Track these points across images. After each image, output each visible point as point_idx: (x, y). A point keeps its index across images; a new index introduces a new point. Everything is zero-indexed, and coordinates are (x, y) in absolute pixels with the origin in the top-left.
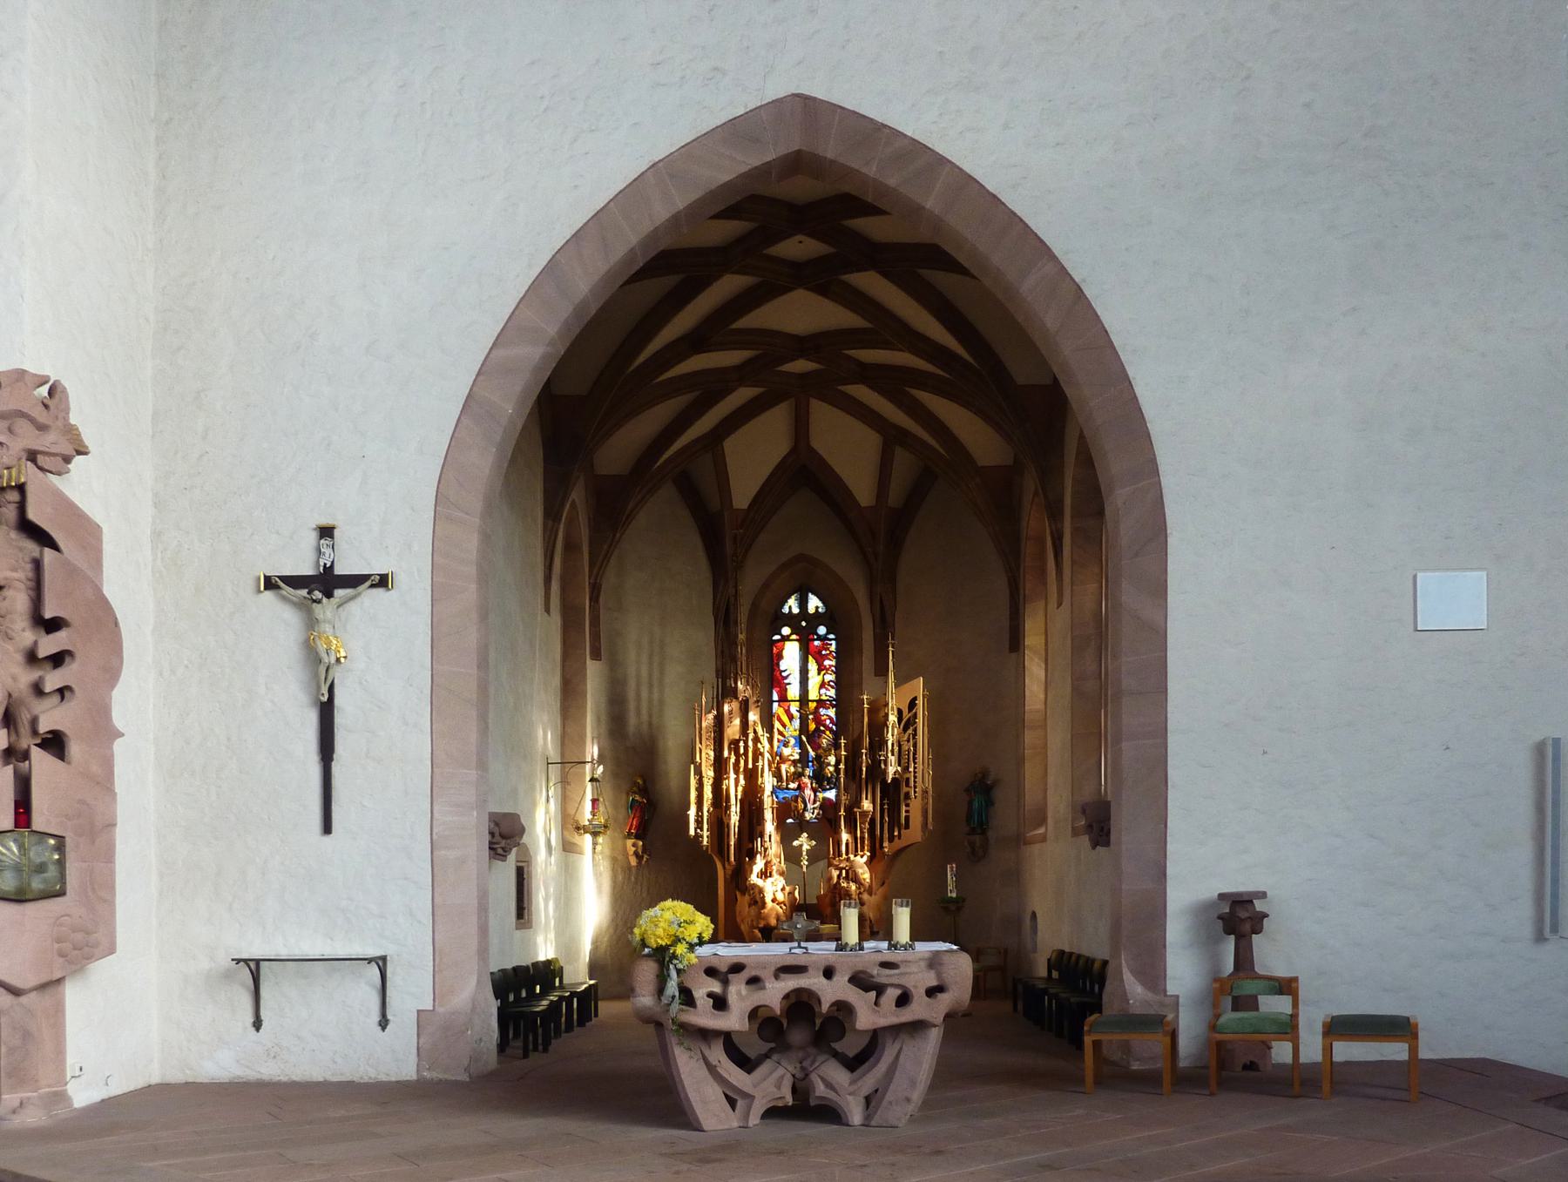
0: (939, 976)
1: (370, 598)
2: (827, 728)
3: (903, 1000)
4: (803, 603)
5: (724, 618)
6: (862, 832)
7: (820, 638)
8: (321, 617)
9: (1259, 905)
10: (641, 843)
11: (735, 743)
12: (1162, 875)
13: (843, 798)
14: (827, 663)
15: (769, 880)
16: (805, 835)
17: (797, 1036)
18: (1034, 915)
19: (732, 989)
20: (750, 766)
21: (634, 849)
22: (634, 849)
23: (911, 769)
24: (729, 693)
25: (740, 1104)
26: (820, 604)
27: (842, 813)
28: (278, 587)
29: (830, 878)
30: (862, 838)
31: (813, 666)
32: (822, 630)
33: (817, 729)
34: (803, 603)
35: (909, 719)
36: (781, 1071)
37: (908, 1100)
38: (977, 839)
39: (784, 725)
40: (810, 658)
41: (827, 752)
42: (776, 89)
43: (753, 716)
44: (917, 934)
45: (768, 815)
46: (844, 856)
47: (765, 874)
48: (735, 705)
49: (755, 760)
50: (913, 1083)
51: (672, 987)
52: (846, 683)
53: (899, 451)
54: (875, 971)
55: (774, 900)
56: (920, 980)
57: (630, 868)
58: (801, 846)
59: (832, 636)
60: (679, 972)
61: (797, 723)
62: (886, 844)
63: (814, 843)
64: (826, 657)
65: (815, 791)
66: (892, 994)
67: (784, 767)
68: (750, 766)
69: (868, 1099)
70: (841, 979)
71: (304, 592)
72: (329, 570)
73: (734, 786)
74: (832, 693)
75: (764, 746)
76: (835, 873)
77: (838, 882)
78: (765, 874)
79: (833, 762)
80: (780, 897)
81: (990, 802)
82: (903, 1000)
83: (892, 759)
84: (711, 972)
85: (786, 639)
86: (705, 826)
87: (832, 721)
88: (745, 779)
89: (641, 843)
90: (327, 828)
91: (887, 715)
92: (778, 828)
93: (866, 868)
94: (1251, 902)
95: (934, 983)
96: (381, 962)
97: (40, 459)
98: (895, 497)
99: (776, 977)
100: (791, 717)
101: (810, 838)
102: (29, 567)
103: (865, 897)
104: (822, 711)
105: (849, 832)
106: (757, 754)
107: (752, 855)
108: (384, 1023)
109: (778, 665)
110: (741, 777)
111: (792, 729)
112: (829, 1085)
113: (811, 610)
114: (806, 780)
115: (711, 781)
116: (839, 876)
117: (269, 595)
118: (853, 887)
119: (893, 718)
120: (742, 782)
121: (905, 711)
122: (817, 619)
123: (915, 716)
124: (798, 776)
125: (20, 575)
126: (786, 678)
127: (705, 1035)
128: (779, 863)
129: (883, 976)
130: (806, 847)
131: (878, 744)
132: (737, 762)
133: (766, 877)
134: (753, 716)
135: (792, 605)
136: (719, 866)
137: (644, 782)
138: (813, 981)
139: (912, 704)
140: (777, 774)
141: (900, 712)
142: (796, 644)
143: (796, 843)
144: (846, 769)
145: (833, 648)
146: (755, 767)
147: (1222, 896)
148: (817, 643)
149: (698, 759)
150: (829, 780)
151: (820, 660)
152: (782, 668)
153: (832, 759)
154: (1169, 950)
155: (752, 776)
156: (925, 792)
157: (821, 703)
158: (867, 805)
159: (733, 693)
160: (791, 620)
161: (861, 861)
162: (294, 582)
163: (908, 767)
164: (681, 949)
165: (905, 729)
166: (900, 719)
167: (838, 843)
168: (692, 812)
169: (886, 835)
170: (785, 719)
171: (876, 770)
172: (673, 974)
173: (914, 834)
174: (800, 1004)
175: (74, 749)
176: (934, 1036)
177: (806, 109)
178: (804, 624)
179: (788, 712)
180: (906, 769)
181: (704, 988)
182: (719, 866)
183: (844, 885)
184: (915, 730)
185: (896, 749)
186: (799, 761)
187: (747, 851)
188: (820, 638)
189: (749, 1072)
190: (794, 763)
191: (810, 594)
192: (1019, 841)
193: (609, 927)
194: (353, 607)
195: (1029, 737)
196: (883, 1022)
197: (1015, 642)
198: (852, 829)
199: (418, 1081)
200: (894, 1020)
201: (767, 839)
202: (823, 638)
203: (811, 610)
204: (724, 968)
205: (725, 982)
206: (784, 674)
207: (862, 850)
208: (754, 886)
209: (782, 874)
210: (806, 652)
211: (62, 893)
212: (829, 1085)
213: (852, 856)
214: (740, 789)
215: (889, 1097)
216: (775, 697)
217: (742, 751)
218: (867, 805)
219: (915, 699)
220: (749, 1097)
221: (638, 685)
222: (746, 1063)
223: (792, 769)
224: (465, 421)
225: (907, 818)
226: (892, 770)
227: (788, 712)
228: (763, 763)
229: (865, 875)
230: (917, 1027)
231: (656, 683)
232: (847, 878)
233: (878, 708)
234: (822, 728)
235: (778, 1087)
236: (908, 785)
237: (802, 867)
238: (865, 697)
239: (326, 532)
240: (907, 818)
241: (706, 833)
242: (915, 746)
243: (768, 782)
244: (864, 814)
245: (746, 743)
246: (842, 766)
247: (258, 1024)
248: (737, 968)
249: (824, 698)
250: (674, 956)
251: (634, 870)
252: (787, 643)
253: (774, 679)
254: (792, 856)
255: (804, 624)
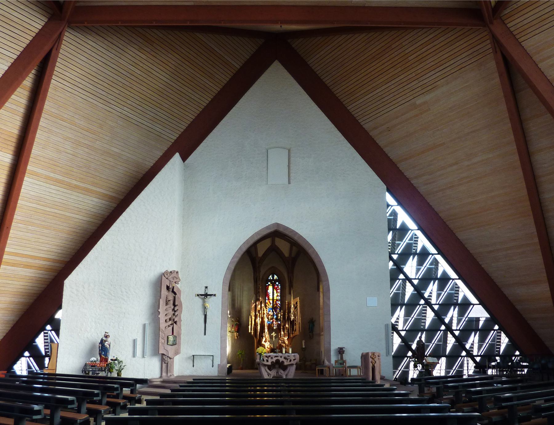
0: (295, 357)
1: (213, 297)
2: (278, 306)
3: (290, 361)
4: (273, 277)
5: (256, 281)
6: (286, 332)
7: (277, 285)
8: (206, 301)
9: (344, 349)
10: (238, 334)
11: (259, 311)
12: (330, 344)
13: (282, 324)
14: (278, 291)
15: (266, 343)
16: (274, 332)
17: (277, 366)
18: (322, 351)
19: (269, 359)
20: (262, 316)
21: (236, 335)
22: (236, 335)
23: (296, 318)
24: (257, 300)
25: (269, 376)
26: (277, 277)
27: (282, 327)
28: (199, 296)
29: (279, 343)
30: (286, 333)
31: (275, 291)
32: (277, 283)
33: (276, 306)
34: (273, 277)
35: (296, 307)
36: (275, 371)
37: (291, 375)
38: (311, 334)
39: (269, 305)
40: (275, 289)
41: (279, 313)
42: (273, 222)
43: (263, 305)
44: (292, 353)
45: (266, 328)
46: (282, 338)
47: (265, 342)
48: (259, 302)
49: (263, 315)
50: (292, 373)
51: (262, 359)
52: (282, 295)
53: (294, 247)
54: (287, 357)
55: (267, 348)
56: (292, 358)
57: (235, 339)
58: (273, 335)
59: (279, 285)
60: (263, 356)
61: (272, 305)
62: (291, 335)
63: (276, 334)
64: (278, 289)
65: (276, 322)
66: (289, 360)
67: (269, 317)
68: (262, 316)
69: (286, 375)
70: (283, 358)
71: (204, 297)
72: (207, 293)
73: (259, 321)
74: (279, 298)
75: (265, 312)
76: (280, 341)
77: (281, 344)
78: (265, 342)
79: (280, 316)
80: (269, 347)
81: (314, 325)
82: (290, 361)
83: (292, 315)
84: (266, 357)
85: (269, 285)
86: (253, 330)
87: (279, 305)
88: (261, 319)
89: (238, 334)
90: (205, 334)
91: (291, 305)
92: (268, 331)
93: (287, 340)
94: (342, 349)
95: (294, 359)
96: (213, 356)
97: (176, 283)
98: (293, 255)
99: (275, 357)
100: (270, 303)
101: (275, 333)
102: (173, 297)
103: (287, 347)
104: (277, 302)
105: (283, 332)
106: (264, 314)
107: (262, 337)
108: (213, 366)
109: (267, 291)
110: (260, 319)
111: (270, 306)
112: (281, 373)
113: (275, 278)
114: (274, 320)
115: (254, 320)
116: (281, 342)
117: (197, 297)
118: (284, 345)
119: (292, 306)
120: (260, 320)
121: (295, 304)
122: (276, 281)
123: (297, 306)
124: (272, 319)
125: (172, 298)
126: (269, 294)
127: (265, 365)
128: (268, 339)
129: (288, 358)
130: (274, 335)
131: (289, 312)
132: (259, 315)
133: (265, 342)
134: (263, 305)
135: (271, 277)
136: (255, 339)
137: (239, 319)
138: (279, 358)
139: (297, 303)
140: (268, 318)
141: (294, 305)
142: (272, 286)
143: (272, 334)
144: (283, 317)
145: (280, 287)
146: (263, 317)
147: (338, 348)
148: (276, 286)
149: (251, 315)
150: (279, 320)
151: (277, 290)
152: (268, 292)
153: (280, 315)
154: (331, 356)
155: (262, 318)
156: (299, 323)
157: (277, 300)
158: (287, 326)
159: (259, 300)
160: (270, 281)
161: (286, 338)
162: (202, 295)
163: (296, 317)
164: (263, 353)
165: (295, 309)
166: (294, 306)
167: (281, 334)
168: (250, 327)
169: (291, 333)
170: (269, 304)
171: (289, 318)
172: (262, 357)
173: (297, 333)
174: (278, 361)
175: (178, 323)
176: (295, 366)
177: (278, 225)
178: (273, 282)
179: (269, 302)
180: (295, 318)
181: (265, 359)
182: (255, 339)
183: (282, 344)
184: (297, 309)
185: (293, 313)
186: (272, 315)
187: (261, 336)
188: (277, 285)
189: (271, 371)
190: (272, 316)
191: (275, 275)
192: (319, 335)
193: (231, 353)
194: (210, 299)
195: (321, 311)
196: (288, 364)
197: (318, 290)
198: (284, 331)
199: (128, 413)
200: (289, 364)
201: (266, 333)
202: (277, 285)
203: (275, 278)
204: (268, 356)
205: (268, 358)
206: (269, 293)
207: (286, 336)
208: (263, 344)
209: (269, 341)
210: (274, 288)
211: (176, 344)
212: (281, 373)
213: (284, 338)
214: (260, 321)
215: (289, 375)
216: (267, 298)
217: (260, 313)
218: (287, 326)
219: (297, 302)
220: (271, 375)
221: (238, 297)
222: (270, 370)
223: (271, 317)
224: (227, 271)
225: (296, 329)
226: (292, 318)
227: (269, 302)
228: (265, 316)
229: (287, 342)
230: (292, 365)
231: (241, 296)
232: (283, 343)
233: (289, 304)
234: (277, 306)
235: (274, 373)
236: (296, 321)
237: (273, 340)
238: (287, 301)
239: (206, 287)
240: (296, 329)
241: (253, 332)
242: (297, 312)
243: (266, 320)
244: (286, 328)
245: (261, 311)
246: (282, 317)
247: (193, 366)
248: (270, 356)
249: (278, 299)
250: (262, 354)
251: (236, 340)
252: (270, 286)
253: (267, 295)
254: (271, 337)
255: (273, 282)
